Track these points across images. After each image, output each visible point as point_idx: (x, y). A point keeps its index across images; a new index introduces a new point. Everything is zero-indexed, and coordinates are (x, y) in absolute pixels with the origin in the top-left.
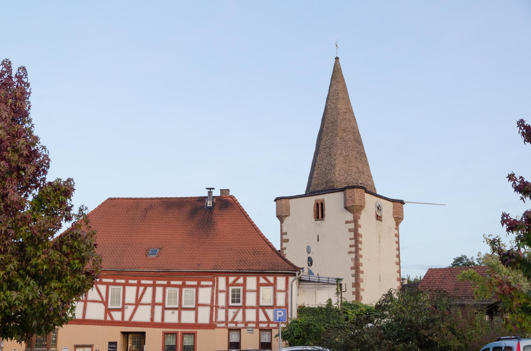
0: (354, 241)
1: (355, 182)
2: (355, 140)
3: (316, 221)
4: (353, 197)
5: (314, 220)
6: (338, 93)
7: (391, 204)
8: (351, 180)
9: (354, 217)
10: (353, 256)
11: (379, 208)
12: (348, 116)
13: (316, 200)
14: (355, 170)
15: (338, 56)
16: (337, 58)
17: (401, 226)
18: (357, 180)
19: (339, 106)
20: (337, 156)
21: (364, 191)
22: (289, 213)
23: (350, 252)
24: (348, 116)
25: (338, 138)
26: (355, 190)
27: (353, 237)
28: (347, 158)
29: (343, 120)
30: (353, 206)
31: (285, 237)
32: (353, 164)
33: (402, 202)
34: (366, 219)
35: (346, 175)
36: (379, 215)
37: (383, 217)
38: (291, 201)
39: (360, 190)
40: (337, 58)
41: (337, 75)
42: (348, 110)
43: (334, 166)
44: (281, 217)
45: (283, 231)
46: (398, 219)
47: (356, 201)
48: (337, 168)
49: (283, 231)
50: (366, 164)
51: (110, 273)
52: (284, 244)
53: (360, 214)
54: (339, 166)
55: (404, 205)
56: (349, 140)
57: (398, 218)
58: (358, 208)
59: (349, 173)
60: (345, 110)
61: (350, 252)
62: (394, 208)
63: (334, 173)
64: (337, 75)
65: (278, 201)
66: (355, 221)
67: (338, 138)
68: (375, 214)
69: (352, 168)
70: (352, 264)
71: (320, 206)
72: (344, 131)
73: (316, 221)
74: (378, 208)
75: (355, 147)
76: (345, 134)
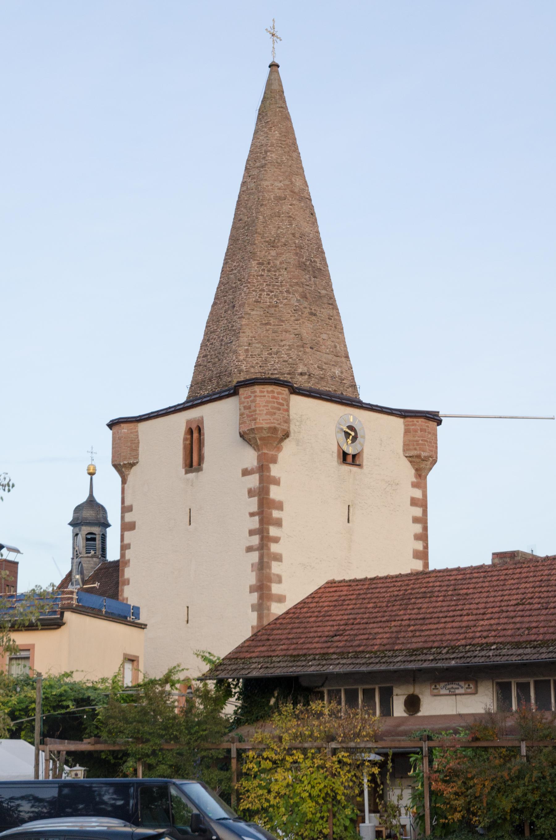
0: (257, 518)
1: (286, 370)
2: (302, 266)
3: (187, 472)
4: (253, 408)
5: (183, 471)
6: (266, 152)
7: (398, 423)
8: (277, 366)
9: (259, 458)
10: (255, 557)
11: (351, 433)
12: (285, 208)
13: (188, 422)
14: (290, 339)
15: (277, 61)
16: (274, 66)
17: (432, 477)
18: (293, 365)
19: (265, 183)
20: (247, 309)
21: (286, 391)
22: (136, 456)
23: (249, 549)
24: (285, 208)
25: (254, 263)
26: (257, 388)
27: (254, 508)
28: (272, 310)
29: (271, 217)
30: (252, 430)
31: (129, 518)
32: (285, 326)
33: (434, 418)
34: (287, 463)
35: (265, 354)
36: (351, 450)
37: (365, 455)
38: (142, 427)
39: (270, 388)
40: (274, 66)
41: (273, 109)
42: (288, 192)
43: (236, 333)
44: (123, 466)
45: (127, 503)
46: (422, 461)
47: (260, 419)
48: (244, 339)
49: (127, 503)
50: (334, 324)
51: (140, 626)
52: (126, 534)
53: (279, 449)
54: (248, 332)
55: (439, 428)
56: (284, 266)
57: (418, 456)
58: (265, 434)
59: (274, 350)
60: (279, 193)
61: (249, 549)
62: (407, 432)
63: (235, 352)
64: (273, 109)
65: (116, 428)
66: (262, 468)
67: (254, 263)
68: (335, 449)
69: (284, 335)
70: (252, 579)
71: (195, 435)
72: (272, 244)
73: (187, 472)
74: (347, 435)
75: (297, 284)
76: (273, 253)
